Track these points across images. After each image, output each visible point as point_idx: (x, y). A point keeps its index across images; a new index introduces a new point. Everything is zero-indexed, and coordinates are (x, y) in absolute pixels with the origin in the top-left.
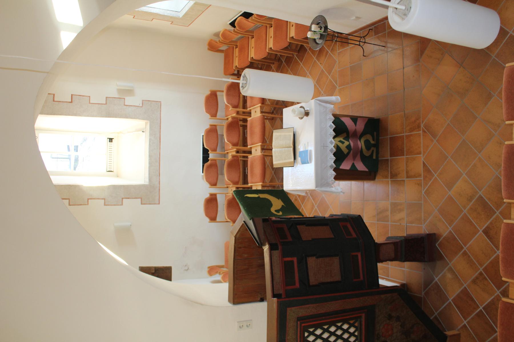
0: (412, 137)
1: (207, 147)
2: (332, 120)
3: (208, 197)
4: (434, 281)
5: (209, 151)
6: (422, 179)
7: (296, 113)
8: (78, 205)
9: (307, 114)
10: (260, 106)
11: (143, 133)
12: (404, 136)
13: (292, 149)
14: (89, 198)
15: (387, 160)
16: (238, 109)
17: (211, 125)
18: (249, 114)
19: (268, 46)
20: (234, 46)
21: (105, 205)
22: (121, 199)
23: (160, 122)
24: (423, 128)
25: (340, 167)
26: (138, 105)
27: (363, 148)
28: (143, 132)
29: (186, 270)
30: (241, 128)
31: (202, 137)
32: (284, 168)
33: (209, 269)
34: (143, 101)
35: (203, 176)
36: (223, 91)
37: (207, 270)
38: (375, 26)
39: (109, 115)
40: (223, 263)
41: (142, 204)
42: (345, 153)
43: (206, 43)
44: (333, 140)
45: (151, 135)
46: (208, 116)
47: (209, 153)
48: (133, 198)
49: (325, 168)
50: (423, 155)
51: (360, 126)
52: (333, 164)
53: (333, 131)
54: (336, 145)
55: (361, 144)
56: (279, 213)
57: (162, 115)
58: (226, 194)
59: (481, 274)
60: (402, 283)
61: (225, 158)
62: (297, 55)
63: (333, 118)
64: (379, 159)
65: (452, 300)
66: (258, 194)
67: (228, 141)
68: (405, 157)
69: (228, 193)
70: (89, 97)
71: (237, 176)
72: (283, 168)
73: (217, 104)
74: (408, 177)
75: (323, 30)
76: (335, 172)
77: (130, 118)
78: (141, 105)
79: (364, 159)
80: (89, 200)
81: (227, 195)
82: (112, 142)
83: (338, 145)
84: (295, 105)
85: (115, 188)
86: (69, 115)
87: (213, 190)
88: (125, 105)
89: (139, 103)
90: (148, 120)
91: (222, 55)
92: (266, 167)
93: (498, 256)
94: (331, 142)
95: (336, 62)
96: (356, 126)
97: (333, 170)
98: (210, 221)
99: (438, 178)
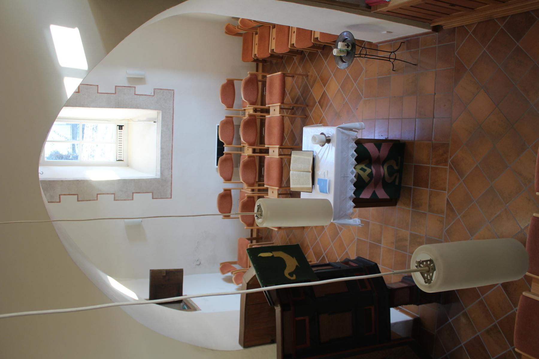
0: (438, 171)
1: (222, 140)
2: (355, 149)
3: (222, 193)
4: (448, 322)
5: (224, 145)
6: (445, 216)
7: (317, 141)
8: (87, 201)
9: (328, 141)
10: (280, 106)
11: (155, 123)
12: (429, 167)
13: (310, 174)
14: (98, 193)
15: (411, 188)
16: (256, 106)
17: (227, 117)
18: (267, 111)
19: (291, 42)
20: (254, 33)
21: (115, 200)
22: (131, 194)
23: (172, 112)
24: (450, 163)
25: (359, 196)
26: (150, 95)
27: (385, 175)
28: (154, 122)
29: (198, 265)
30: (260, 83)
31: (217, 127)
32: (301, 192)
33: (221, 265)
34: (154, 89)
35: (217, 168)
36: (239, 218)
37: (219, 266)
38: (408, 39)
39: (119, 105)
40: (235, 259)
41: (153, 198)
42: (366, 181)
43: (224, 27)
44: (354, 170)
45: (163, 126)
46: (224, 106)
47: (224, 146)
48: (144, 193)
49: (345, 199)
50: (448, 192)
51: (384, 152)
52: (355, 153)
53: (355, 160)
54: (357, 174)
55: (384, 170)
56: (292, 276)
57: (174, 104)
58: (241, 189)
59: (495, 326)
60: (415, 316)
61: (241, 151)
62: (321, 52)
63: (355, 146)
64: (404, 163)
65: (464, 345)
66: (272, 253)
67: (244, 140)
68: (429, 189)
69: (243, 189)
70: (97, 86)
71: (252, 177)
72: (300, 192)
73: (234, 100)
74: (430, 211)
75: (350, 48)
76: (354, 203)
77: (141, 109)
78: (153, 94)
79: (386, 186)
80: (99, 195)
81: (242, 190)
82: (122, 129)
83: (359, 173)
84: (310, 226)
85: (125, 182)
86: (76, 106)
87: (228, 186)
88: (135, 94)
89: (150, 92)
90: (160, 110)
91: (241, 39)
92: (283, 166)
93: (514, 314)
94: (352, 172)
95: (364, 69)
96: (379, 152)
97: (353, 201)
98: (224, 218)
99: (461, 220)
